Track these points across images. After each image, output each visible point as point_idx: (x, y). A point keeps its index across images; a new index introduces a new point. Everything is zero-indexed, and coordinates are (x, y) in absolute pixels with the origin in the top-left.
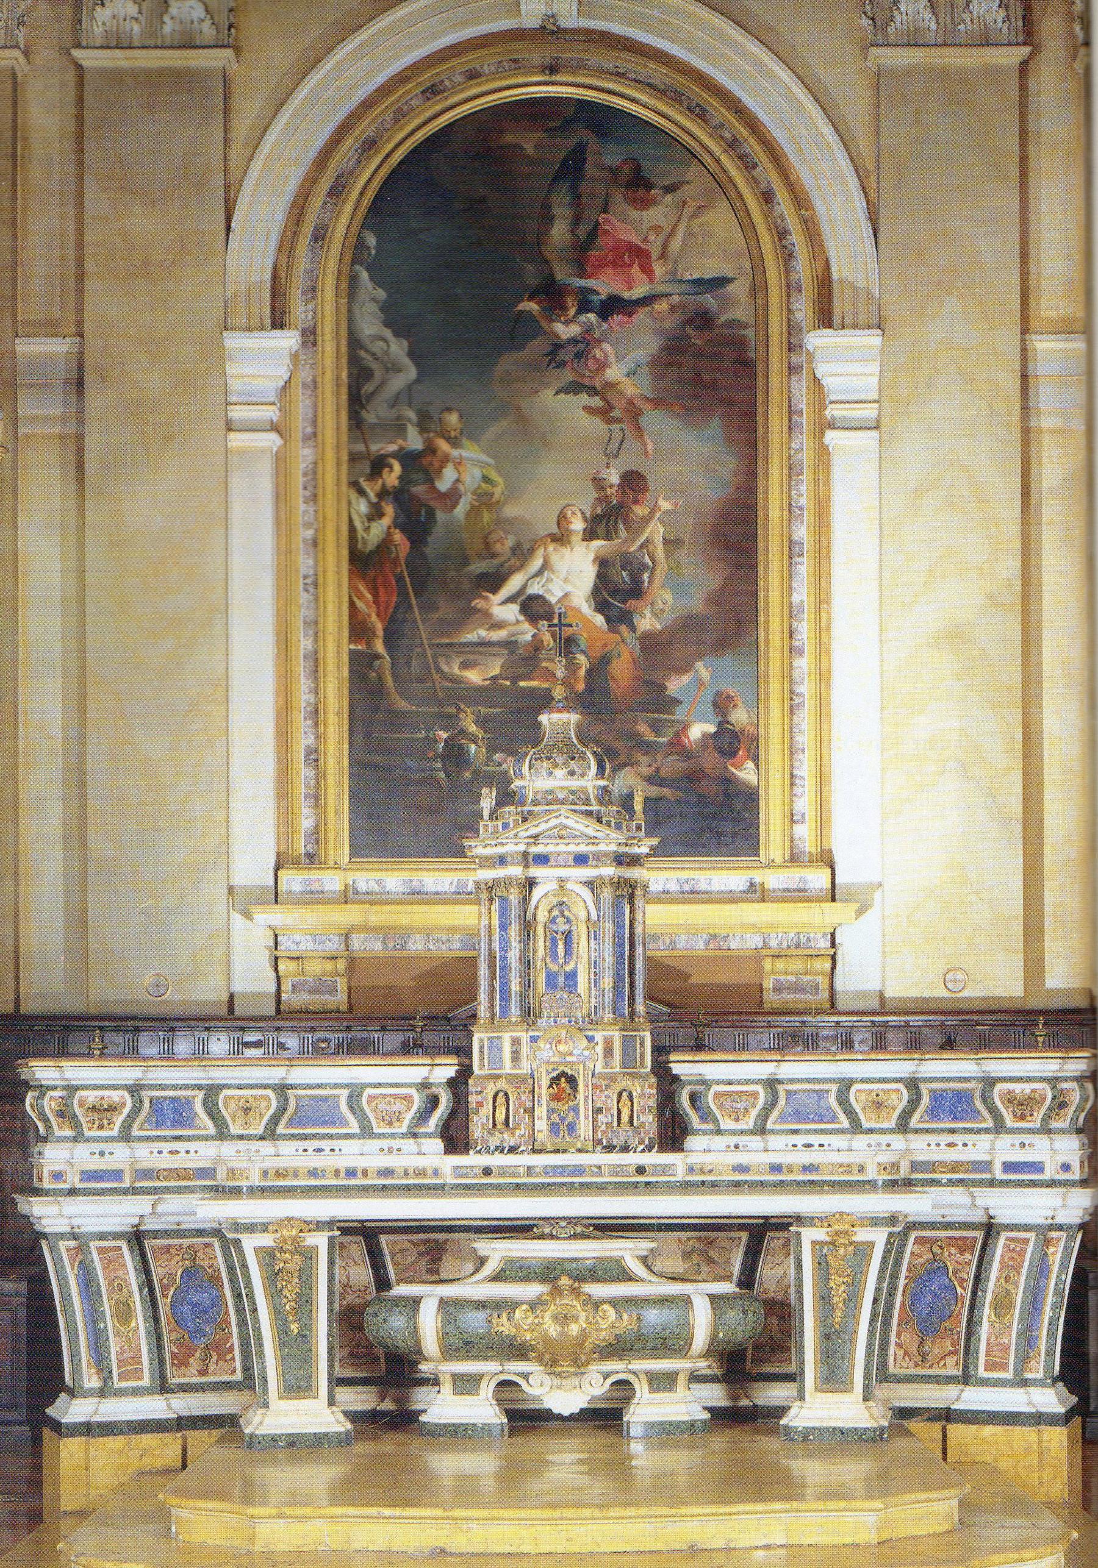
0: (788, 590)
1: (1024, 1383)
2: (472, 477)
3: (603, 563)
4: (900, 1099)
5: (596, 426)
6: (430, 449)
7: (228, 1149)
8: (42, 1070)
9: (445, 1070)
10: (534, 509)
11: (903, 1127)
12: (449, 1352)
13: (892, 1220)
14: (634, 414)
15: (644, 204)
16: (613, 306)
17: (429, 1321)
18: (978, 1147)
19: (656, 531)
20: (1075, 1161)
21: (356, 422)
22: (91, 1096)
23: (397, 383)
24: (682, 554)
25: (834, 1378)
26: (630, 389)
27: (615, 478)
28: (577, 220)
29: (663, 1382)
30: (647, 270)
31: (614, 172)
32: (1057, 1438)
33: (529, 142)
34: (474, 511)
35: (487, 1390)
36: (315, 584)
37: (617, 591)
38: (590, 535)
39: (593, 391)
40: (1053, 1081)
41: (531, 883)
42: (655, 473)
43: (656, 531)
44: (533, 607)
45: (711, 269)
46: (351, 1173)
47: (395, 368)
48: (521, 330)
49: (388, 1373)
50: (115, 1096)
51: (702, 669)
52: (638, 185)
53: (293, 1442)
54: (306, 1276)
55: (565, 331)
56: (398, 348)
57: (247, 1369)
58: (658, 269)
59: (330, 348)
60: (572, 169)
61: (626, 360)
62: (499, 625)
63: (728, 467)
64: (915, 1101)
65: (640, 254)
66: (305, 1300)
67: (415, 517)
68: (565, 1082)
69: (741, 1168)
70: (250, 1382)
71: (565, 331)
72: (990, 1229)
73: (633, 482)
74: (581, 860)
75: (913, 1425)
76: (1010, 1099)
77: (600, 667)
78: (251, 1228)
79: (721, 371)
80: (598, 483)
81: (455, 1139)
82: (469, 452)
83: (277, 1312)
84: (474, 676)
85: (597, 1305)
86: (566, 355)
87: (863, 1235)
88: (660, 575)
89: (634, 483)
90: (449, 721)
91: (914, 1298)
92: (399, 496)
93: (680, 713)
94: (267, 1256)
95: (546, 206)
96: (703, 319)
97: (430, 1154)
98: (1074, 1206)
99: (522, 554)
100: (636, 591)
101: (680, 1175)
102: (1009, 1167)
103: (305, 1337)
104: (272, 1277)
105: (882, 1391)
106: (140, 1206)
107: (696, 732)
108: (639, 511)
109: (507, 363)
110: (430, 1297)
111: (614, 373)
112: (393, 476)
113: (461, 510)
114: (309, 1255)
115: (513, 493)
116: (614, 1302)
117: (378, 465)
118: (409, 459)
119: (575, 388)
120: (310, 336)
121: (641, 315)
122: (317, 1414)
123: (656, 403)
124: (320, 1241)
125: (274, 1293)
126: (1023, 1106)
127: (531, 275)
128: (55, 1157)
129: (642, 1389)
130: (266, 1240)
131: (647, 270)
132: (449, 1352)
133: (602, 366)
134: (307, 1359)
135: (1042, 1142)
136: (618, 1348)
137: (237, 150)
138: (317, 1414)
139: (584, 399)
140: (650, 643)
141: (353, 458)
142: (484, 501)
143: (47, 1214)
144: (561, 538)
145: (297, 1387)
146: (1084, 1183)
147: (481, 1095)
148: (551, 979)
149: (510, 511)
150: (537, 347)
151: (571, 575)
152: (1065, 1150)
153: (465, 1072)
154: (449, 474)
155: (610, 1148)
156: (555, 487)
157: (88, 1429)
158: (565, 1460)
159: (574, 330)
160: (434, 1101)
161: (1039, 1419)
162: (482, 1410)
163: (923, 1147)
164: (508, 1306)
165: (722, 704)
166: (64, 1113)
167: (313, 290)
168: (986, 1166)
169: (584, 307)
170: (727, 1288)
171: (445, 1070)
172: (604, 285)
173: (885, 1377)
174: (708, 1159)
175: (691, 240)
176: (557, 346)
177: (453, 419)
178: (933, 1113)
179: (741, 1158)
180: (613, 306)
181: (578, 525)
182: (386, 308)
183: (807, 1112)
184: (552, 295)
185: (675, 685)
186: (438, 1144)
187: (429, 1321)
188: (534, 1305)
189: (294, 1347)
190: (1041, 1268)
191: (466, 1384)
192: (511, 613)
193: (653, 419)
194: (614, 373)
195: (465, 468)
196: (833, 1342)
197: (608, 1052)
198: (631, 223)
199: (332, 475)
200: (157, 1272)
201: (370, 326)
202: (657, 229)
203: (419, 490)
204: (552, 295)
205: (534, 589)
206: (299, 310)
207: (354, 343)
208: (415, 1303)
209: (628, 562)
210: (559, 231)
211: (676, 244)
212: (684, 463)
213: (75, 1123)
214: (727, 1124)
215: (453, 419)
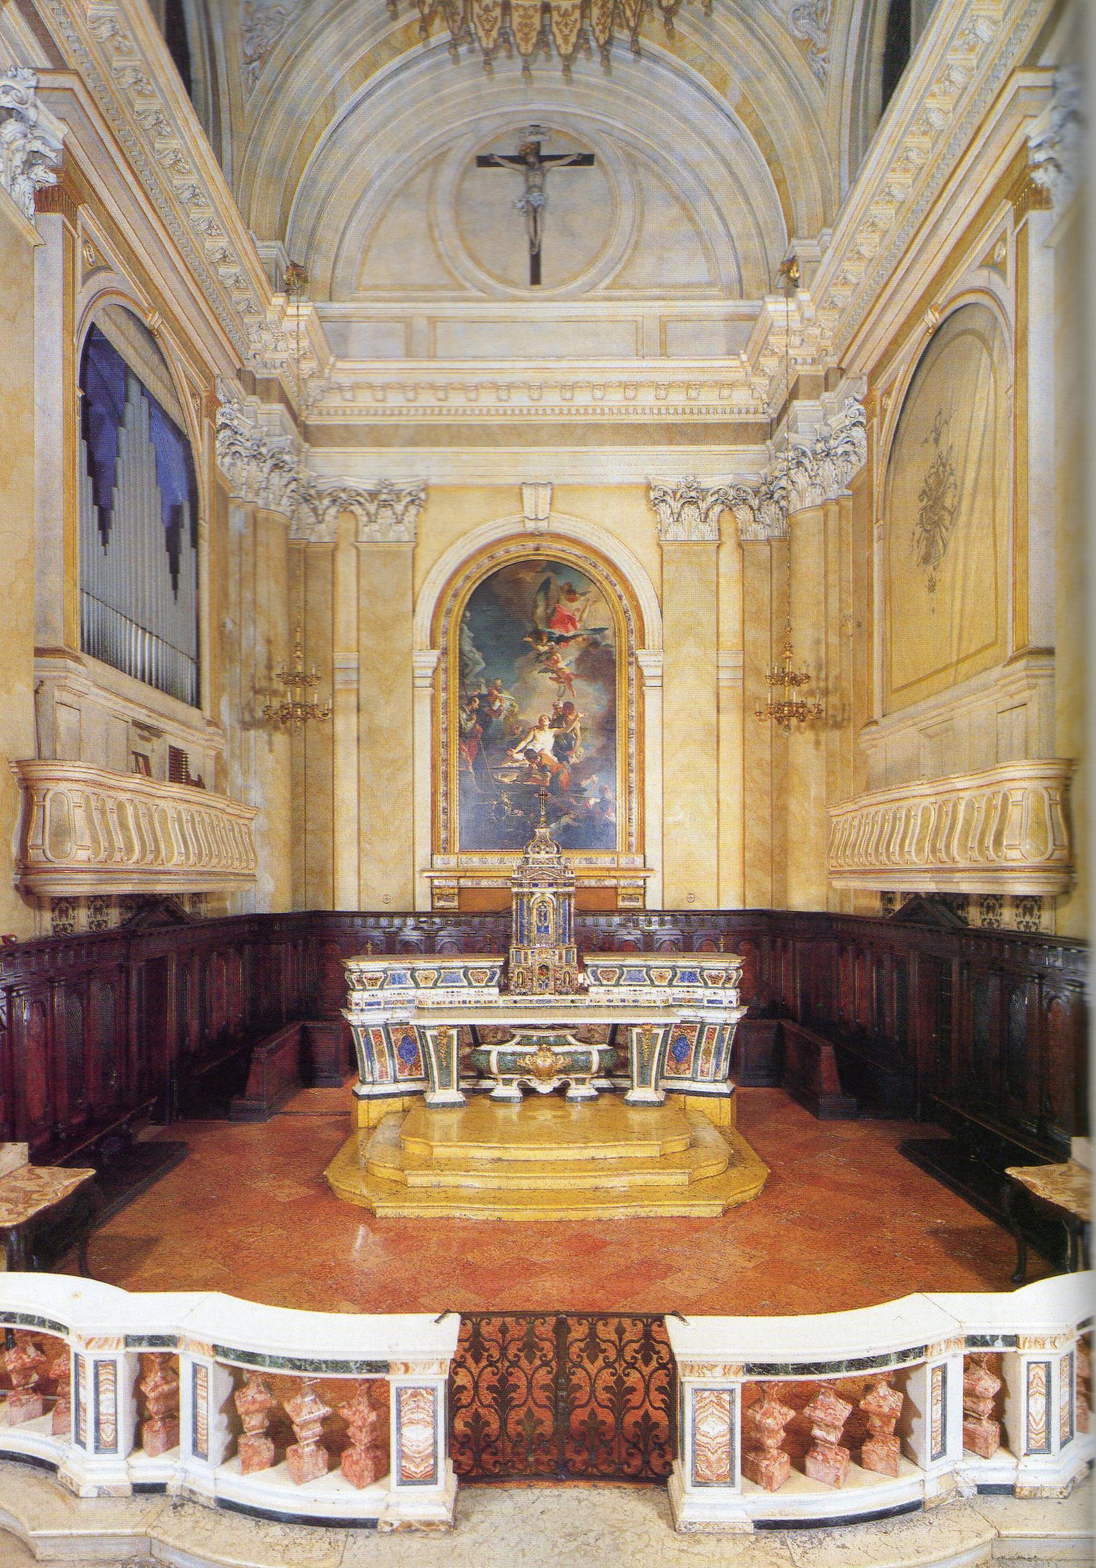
0: (627, 747)
1: (715, 1081)
2: (506, 704)
3: (556, 737)
4: (669, 974)
5: (554, 685)
6: (490, 694)
7: (419, 992)
8: (352, 965)
9: (500, 961)
10: (530, 717)
11: (670, 985)
12: (501, 1072)
13: (666, 1025)
14: (568, 679)
15: (572, 600)
16: (561, 640)
17: (494, 1058)
18: (700, 993)
19: (577, 725)
20: (734, 1000)
21: (462, 684)
22: (369, 975)
23: (478, 669)
24: (587, 734)
25: (644, 1082)
26: (567, 671)
27: (561, 705)
28: (547, 606)
29: (582, 1081)
30: (575, 627)
31: (562, 588)
32: (727, 1103)
33: (528, 577)
34: (506, 718)
35: (515, 1083)
36: (446, 745)
37: (562, 748)
38: (551, 727)
39: (553, 672)
40: (726, 970)
41: (532, 894)
42: (577, 703)
43: (577, 725)
44: (529, 754)
45: (599, 625)
46: (464, 1002)
47: (476, 663)
48: (526, 648)
49: (474, 1070)
50: (378, 975)
51: (595, 778)
52: (571, 593)
53: (444, 1105)
54: (449, 1046)
55: (543, 649)
56: (478, 656)
57: (426, 1073)
58: (578, 625)
59: (453, 659)
60: (545, 586)
61: (566, 659)
62: (517, 761)
63: (605, 699)
64: (674, 976)
65: (571, 620)
66: (449, 1053)
67: (484, 717)
68: (544, 968)
69: (610, 1001)
70: (427, 1078)
71: (543, 649)
72: (703, 1024)
73: (569, 707)
74: (551, 885)
75: (674, 1096)
76: (710, 977)
77: (555, 777)
78: (430, 1028)
79: (601, 662)
80: (555, 707)
81: (504, 989)
82: (505, 695)
83: (438, 1057)
84: (506, 780)
85: (556, 1054)
86: (543, 658)
87: (655, 1031)
88: (579, 742)
89: (569, 707)
90: (497, 797)
91: (673, 1049)
92: (478, 711)
93: (586, 794)
94: (434, 1038)
95: (535, 602)
96: (595, 644)
97: (492, 993)
98: (735, 1016)
99: (525, 733)
100: (570, 748)
101: (587, 1003)
102: (709, 1002)
103: (448, 1067)
104: (437, 1046)
105: (664, 1084)
106: (387, 1015)
107: (592, 802)
108: (571, 717)
109: (520, 662)
110: (495, 1050)
111: (562, 665)
112: (476, 704)
113: (502, 717)
114: (451, 1037)
115: (522, 710)
116: (563, 1054)
117: (471, 700)
118: (481, 697)
119: (545, 671)
120: (445, 652)
121: (572, 643)
122: (453, 1095)
123: (577, 676)
124: (454, 1032)
125: (437, 1052)
126: (715, 979)
127: (529, 627)
128: (356, 996)
129: (573, 1084)
130: (435, 1032)
131: (575, 627)
132: (501, 1072)
133: (557, 662)
134: (449, 1074)
135: (721, 992)
136: (565, 1071)
137: (418, 581)
138: (453, 1095)
139: (550, 675)
140: (574, 767)
141: (460, 697)
142: (512, 713)
143: (354, 1018)
144: (541, 727)
145: (445, 1085)
146: (737, 1008)
147: (515, 971)
148: (539, 928)
149: (521, 717)
150: (532, 655)
151: (544, 741)
152: (731, 995)
153: (507, 963)
154: (498, 704)
155: (561, 993)
156: (539, 708)
157: (369, 1097)
158: (545, 1115)
159: (546, 648)
160: (494, 974)
161: (720, 1095)
162: (513, 1091)
163: (678, 992)
164: (523, 1055)
165: (602, 791)
166: (360, 981)
167: (445, 633)
168: (701, 1001)
169: (550, 639)
170: (605, 1047)
171: (500, 961)
172: (557, 632)
173: (663, 1077)
174: (597, 997)
175: (591, 614)
176: (540, 655)
177: (499, 682)
178: (682, 979)
179: (610, 997)
180: (561, 640)
181: (547, 722)
182: (473, 639)
183: (636, 980)
184: (538, 635)
185: (584, 783)
186: (497, 990)
187: (494, 1058)
188: (533, 1055)
189: (445, 1069)
190: (721, 1040)
191: (507, 1082)
192: (520, 756)
193: (577, 683)
194: (562, 665)
195: (504, 701)
196: (644, 1067)
197: (560, 958)
198: (569, 608)
199: (454, 707)
200: (393, 1038)
201: (468, 647)
202: (578, 610)
203: (486, 709)
204: (538, 635)
205: (530, 747)
206: (441, 641)
207: (461, 653)
208: (489, 1052)
209: (566, 736)
210: (540, 611)
211: (585, 615)
212: (587, 700)
213: (363, 984)
214: (605, 982)
215: (499, 682)
